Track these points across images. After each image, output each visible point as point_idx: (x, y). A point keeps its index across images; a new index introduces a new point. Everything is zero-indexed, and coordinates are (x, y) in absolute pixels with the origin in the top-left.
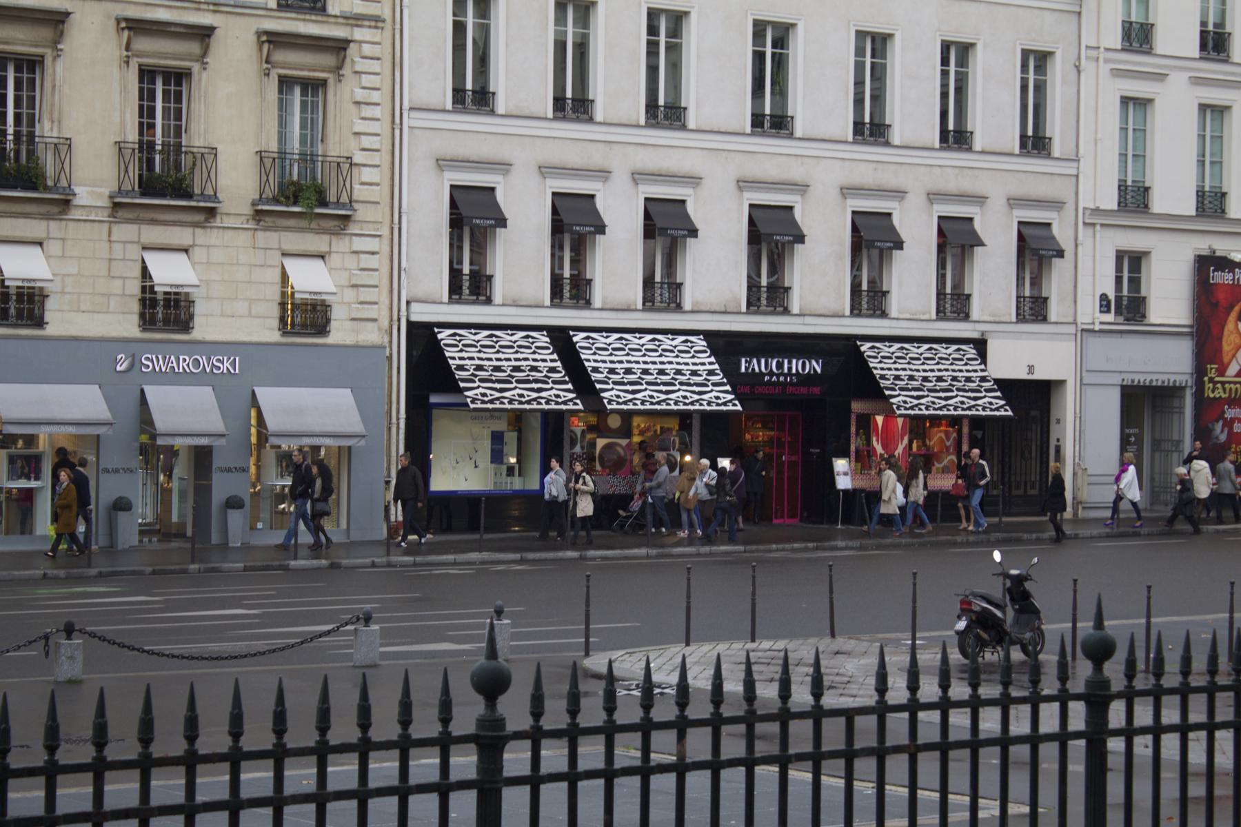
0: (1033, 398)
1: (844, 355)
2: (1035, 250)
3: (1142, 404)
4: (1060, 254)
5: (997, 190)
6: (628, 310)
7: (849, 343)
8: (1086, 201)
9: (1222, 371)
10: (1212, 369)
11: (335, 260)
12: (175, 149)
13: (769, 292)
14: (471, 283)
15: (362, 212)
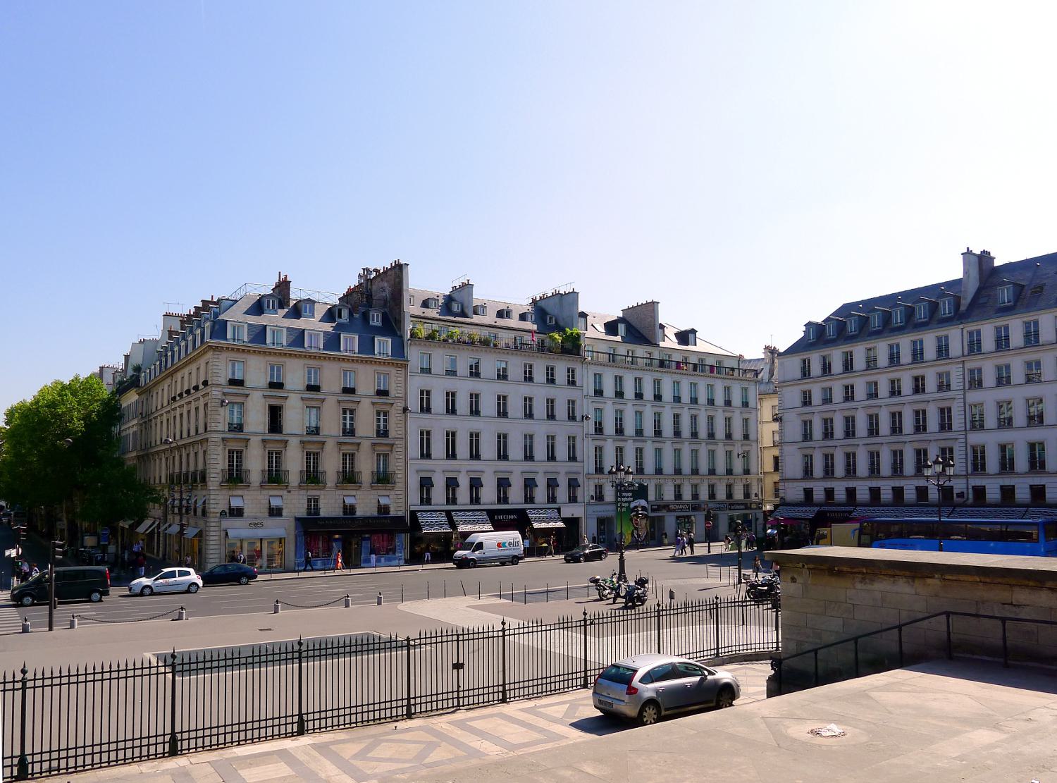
2: (573, 484)
4: (579, 486)
5: (562, 470)
12: (352, 471)
13: (503, 499)
14: (426, 500)
15: (363, 485)
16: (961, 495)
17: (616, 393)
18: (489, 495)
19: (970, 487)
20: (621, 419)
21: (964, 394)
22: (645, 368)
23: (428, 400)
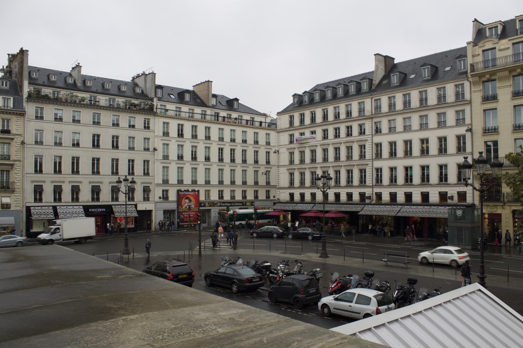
0: (149, 213)
1: (109, 208)
3: (167, 213)
6: (69, 202)
7: (110, 206)
8: (156, 182)
9: (182, 207)
10: (180, 207)
11: (12, 197)
12: (8, 182)
15: (16, 190)
16: (369, 198)
17: (192, 136)
18: (85, 196)
19: (374, 193)
20: (195, 152)
21: (372, 137)
22: (176, 117)
23: (117, 142)
